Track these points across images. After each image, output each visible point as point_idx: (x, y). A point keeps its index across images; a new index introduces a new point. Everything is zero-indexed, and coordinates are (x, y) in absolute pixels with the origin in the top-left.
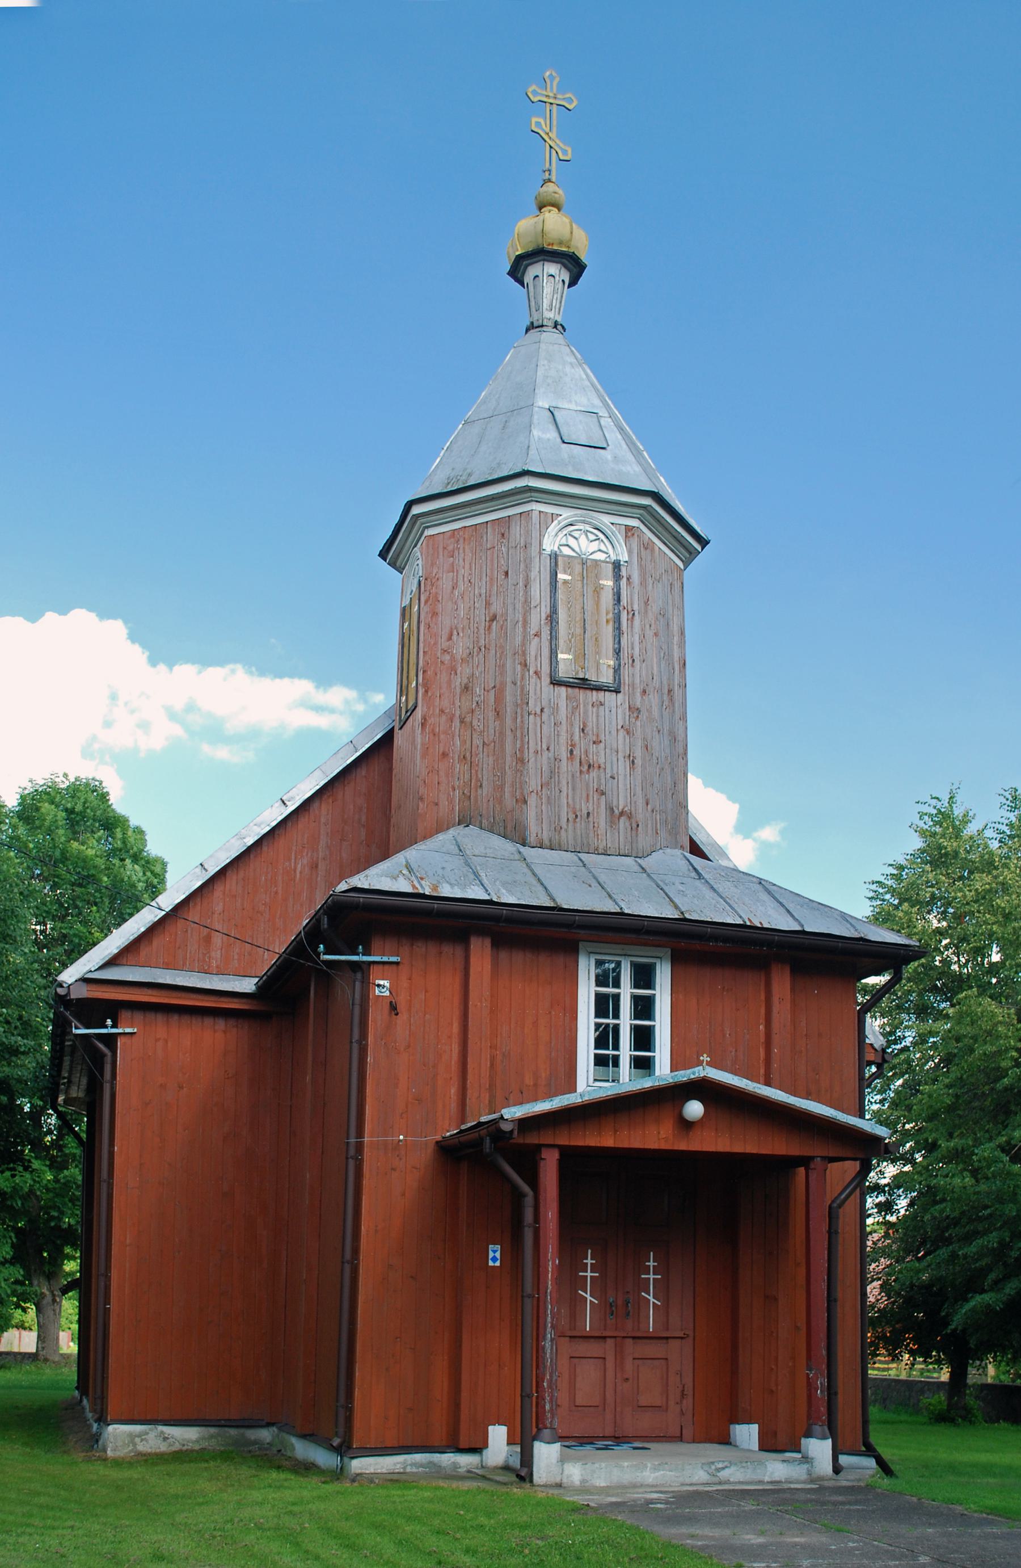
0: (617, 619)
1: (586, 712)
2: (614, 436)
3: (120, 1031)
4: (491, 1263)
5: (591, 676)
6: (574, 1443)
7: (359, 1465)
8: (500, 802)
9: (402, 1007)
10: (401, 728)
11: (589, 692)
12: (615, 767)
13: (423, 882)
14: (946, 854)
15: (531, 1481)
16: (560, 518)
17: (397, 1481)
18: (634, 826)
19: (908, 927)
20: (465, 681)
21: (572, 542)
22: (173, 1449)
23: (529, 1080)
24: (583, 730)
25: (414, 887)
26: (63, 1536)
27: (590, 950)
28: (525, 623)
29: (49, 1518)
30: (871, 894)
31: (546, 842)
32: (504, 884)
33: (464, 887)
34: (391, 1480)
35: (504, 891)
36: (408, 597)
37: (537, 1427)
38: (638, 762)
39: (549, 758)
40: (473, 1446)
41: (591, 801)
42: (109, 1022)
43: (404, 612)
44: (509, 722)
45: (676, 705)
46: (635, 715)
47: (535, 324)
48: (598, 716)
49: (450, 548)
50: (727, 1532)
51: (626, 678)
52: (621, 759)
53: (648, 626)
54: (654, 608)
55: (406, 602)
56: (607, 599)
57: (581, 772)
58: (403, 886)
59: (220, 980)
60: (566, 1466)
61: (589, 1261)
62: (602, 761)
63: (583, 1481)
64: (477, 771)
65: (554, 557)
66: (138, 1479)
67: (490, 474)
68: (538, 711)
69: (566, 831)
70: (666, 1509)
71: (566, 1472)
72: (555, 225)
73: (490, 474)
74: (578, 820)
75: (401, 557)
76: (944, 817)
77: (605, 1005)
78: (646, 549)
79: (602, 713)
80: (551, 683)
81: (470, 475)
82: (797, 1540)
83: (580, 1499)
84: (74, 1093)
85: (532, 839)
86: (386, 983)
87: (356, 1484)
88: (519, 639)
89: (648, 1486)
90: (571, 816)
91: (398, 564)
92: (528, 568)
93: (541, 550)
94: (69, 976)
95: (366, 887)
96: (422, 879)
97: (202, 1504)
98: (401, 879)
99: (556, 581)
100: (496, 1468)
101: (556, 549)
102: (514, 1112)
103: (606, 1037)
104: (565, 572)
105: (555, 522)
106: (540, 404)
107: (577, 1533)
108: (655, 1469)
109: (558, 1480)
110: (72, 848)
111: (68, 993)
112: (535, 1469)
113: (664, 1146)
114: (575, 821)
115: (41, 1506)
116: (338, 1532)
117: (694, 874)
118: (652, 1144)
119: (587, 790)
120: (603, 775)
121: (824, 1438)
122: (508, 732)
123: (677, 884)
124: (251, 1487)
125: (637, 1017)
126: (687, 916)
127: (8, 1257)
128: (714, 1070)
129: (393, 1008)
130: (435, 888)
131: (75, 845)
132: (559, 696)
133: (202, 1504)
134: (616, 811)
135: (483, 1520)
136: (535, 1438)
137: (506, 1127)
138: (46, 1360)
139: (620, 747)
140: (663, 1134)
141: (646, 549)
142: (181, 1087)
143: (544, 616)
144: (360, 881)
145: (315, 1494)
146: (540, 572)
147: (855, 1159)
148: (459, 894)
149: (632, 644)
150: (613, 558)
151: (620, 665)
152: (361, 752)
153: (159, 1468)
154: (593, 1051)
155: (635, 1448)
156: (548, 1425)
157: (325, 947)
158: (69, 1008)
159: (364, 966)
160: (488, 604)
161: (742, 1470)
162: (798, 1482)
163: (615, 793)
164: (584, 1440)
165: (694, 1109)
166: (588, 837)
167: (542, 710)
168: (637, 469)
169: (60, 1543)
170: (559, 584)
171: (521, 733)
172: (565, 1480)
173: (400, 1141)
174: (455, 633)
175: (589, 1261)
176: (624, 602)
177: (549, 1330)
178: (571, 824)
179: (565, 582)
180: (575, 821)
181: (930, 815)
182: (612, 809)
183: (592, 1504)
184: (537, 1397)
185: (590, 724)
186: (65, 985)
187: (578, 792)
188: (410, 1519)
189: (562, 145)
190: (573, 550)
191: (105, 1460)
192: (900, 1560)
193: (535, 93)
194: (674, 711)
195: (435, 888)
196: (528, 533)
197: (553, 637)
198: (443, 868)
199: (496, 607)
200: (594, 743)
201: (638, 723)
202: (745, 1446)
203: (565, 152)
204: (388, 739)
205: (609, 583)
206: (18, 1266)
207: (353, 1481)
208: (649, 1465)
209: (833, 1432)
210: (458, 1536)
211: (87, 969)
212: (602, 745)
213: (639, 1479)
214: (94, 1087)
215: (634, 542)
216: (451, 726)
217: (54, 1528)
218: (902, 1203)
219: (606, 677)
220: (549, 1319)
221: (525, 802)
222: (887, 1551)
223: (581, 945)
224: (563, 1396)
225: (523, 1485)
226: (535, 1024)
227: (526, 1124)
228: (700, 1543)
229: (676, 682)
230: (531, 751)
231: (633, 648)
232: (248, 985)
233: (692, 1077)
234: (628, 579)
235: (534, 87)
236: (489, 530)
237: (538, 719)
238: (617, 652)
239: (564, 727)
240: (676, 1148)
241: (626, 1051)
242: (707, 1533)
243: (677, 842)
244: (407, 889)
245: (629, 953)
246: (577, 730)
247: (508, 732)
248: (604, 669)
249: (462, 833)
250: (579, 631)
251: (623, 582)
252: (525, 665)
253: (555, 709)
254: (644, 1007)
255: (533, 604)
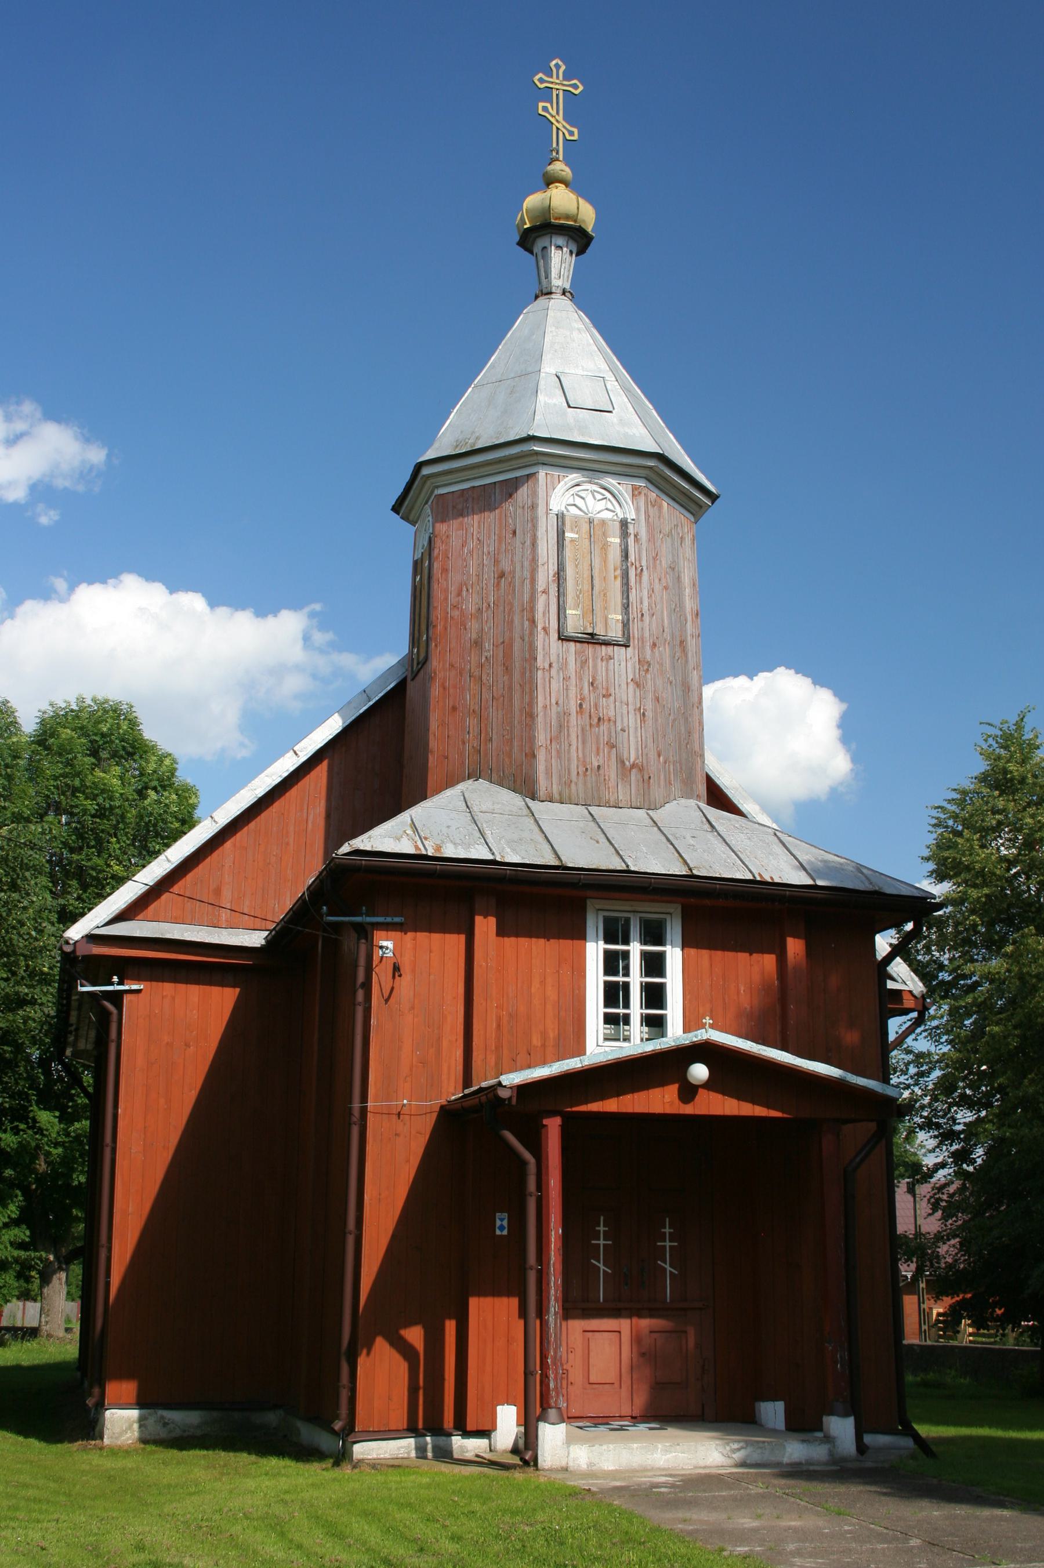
0: (625, 575)
1: (595, 666)
2: (620, 400)
3: (126, 987)
4: (498, 1232)
5: (599, 630)
6: (588, 1424)
7: (363, 1450)
8: (510, 756)
9: (406, 969)
10: (413, 679)
11: (598, 647)
12: (625, 720)
13: (426, 843)
14: (1012, 779)
15: (536, 1464)
16: (566, 479)
17: (399, 1466)
18: (646, 777)
19: (971, 855)
20: (474, 636)
21: (579, 502)
22: (173, 1435)
23: (536, 1041)
24: (592, 684)
25: (417, 847)
26: (47, 1529)
27: (598, 907)
28: (533, 581)
29: (35, 1511)
30: (934, 821)
31: (556, 796)
32: (510, 843)
33: (468, 846)
34: (392, 1466)
35: (509, 850)
36: (421, 551)
37: (541, 1406)
38: (649, 714)
39: (558, 713)
40: (480, 1428)
41: (601, 754)
42: (115, 979)
43: (416, 564)
44: (517, 676)
45: (690, 655)
46: (646, 667)
47: (545, 291)
48: (607, 670)
49: (460, 507)
50: (724, 1516)
51: (635, 629)
52: (632, 712)
53: (657, 581)
54: (665, 562)
55: (418, 556)
56: (614, 555)
57: (591, 725)
58: (406, 847)
59: (229, 934)
60: (572, 1448)
61: (602, 1228)
62: (612, 714)
63: (590, 1464)
64: (486, 725)
65: (561, 517)
66: (131, 1469)
67: (498, 438)
68: (547, 666)
69: (576, 784)
70: (669, 1493)
71: (572, 1455)
72: (562, 200)
73: (498, 438)
74: (589, 773)
75: (413, 512)
76: (1007, 740)
77: (613, 963)
78: (654, 506)
79: (611, 667)
80: (559, 638)
81: (478, 438)
82: (793, 1523)
83: (583, 1484)
84: (82, 1045)
85: (542, 792)
86: (389, 944)
87: (356, 1471)
88: (526, 597)
89: (659, 1469)
90: (581, 770)
91: (411, 518)
92: (535, 527)
93: (548, 510)
94: (76, 932)
95: (368, 848)
96: (426, 839)
97: (194, 1493)
98: (405, 839)
99: (564, 539)
100: (505, 1451)
101: (563, 509)
102: (513, 1079)
103: (614, 994)
104: (572, 531)
105: (562, 483)
106: (547, 370)
107: (567, 1518)
108: (666, 1451)
109: (564, 1464)
110: (92, 781)
111: (74, 951)
112: (539, 1453)
113: (669, 1110)
114: (585, 775)
115: (28, 1500)
116: (327, 1521)
117: (707, 826)
118: (657, 1108)
119: (598, 743)
120: (613, 728)
121: (845, 1415)
122: (517, 687)
123: (688, 837)
124: (246, 1475)
125: (648, 974)
126: (695, 872)
127: (13, 1216)
128: (718, 1033)
129: (396, 969)
130: (438, 848)
131: (98, 773)
132: (568, 650)
133: (194, 1493)
134: (627, 763)
135: (476, 1506)
136: (543, 1417)
137: (504, 1094)
138: (49, 1336)
139: (631, 700)
140: (667, 1098)
141: (654, 506)
142: (187, 1045)
143: (551, 573)
144: (366, 842)
145: (310, 1481)
146: (547, 531)
147: (872, 1121)
148: (462, 855)
149: (641, 599)
150: (621, 516)
151: (628, 620)
152: (374, 701)
153: (156, 1456)
154: (602, 1010)
155: (651, 1429)
156: (553, 1404)
157: (329, 909)
158: (77, 964)
159: (369, 928)
160: (496, 562)
161: (759, 1451)
162: (819, 1463)
163: (626, 745)
164: (600, 1420)
165: (699, 1072)
166: (598, 790)
167: (550, 665)
168: (643, 431)
169: (43, 1537)
170: (567, 542)
171: (529, 687)
172: (571, 1464)
173: (404, 1105)
174: (464, 589)
175: (602, 1228)
176: (632, 558)
177: (552, 1303)
178: (581, 777)
179: (572, 541)
180: (585, 775)
181: (995, 738)
182: (623, 762)
183: (594, 1489)
184: (541, 1375)
185: (599, 678)
186: (71, 942)
187: (588, 745)
188: (401, 1506)
189: (568, 127)
190: (580, 509)
191: (101, 1449)
192: (890, 1542)
193: (541, 81)
194: (687, 662)
195: (438, 848)
196: (535, 494)
197: (561, 594)
198: (448, 827)
199: (505, 565)
200: (604, 696)
201: (649, 676)
202: (770, 1425)
203: (571, 133)
204: (401, 688)
205: (615, 540)
206: (24, 1226)
207: (354, 1467)
208: (660, 1446)
209: (852, 1408)
210: (447, 1523)
211: (94, 924)
212: (612, 698)
213: (649, 1462)
214: (102, 1042)
215: (642, 499)
216: (460, 680)
217: (38, 1521)
218: (979, 1153)
219: (615, 633)
220: (552, 1292)
221: (534, 756)
222: (880, 1534)
223: (589, 902)
224: (576, 1375)
225: (527, 1469)
226: (543, 982)
227: (524, 1090)
228: (691, 1528)
229: (689, 632)
230: (540, 705)
231: (641, 603)
232: (256, 939)
233: (695, 1039)
234: (635, 536)
235: (540, 75)
236: (497, 491)
237: (547, 674)
238: (626, 607)
239: (573, 681)
240: (681, 1112)
241: (636, 1009)
242: (702, 1517)
243: (692, 789)
244: (411, 850)
245: (640, 909)
246: (586, 685)
247: (518, 687)
248: (612, 624)
249: (470, 788)
250: (587, 587)
251: (631, 540)
252: (533, 622)
253: (563, 667)
254: (654, 964)
255: (540, 562)
